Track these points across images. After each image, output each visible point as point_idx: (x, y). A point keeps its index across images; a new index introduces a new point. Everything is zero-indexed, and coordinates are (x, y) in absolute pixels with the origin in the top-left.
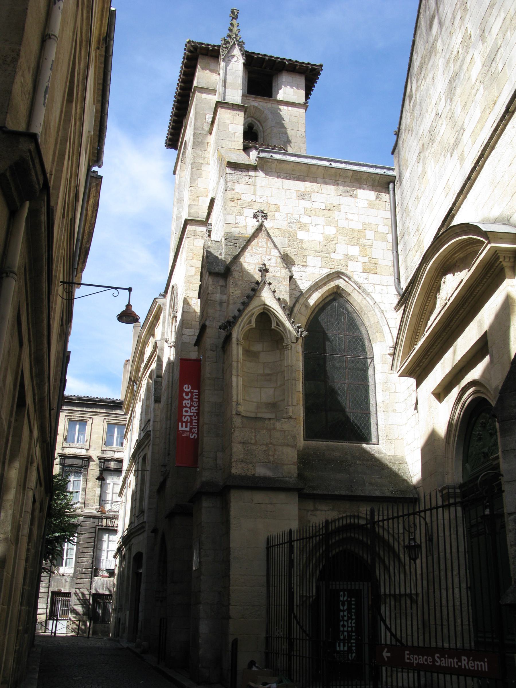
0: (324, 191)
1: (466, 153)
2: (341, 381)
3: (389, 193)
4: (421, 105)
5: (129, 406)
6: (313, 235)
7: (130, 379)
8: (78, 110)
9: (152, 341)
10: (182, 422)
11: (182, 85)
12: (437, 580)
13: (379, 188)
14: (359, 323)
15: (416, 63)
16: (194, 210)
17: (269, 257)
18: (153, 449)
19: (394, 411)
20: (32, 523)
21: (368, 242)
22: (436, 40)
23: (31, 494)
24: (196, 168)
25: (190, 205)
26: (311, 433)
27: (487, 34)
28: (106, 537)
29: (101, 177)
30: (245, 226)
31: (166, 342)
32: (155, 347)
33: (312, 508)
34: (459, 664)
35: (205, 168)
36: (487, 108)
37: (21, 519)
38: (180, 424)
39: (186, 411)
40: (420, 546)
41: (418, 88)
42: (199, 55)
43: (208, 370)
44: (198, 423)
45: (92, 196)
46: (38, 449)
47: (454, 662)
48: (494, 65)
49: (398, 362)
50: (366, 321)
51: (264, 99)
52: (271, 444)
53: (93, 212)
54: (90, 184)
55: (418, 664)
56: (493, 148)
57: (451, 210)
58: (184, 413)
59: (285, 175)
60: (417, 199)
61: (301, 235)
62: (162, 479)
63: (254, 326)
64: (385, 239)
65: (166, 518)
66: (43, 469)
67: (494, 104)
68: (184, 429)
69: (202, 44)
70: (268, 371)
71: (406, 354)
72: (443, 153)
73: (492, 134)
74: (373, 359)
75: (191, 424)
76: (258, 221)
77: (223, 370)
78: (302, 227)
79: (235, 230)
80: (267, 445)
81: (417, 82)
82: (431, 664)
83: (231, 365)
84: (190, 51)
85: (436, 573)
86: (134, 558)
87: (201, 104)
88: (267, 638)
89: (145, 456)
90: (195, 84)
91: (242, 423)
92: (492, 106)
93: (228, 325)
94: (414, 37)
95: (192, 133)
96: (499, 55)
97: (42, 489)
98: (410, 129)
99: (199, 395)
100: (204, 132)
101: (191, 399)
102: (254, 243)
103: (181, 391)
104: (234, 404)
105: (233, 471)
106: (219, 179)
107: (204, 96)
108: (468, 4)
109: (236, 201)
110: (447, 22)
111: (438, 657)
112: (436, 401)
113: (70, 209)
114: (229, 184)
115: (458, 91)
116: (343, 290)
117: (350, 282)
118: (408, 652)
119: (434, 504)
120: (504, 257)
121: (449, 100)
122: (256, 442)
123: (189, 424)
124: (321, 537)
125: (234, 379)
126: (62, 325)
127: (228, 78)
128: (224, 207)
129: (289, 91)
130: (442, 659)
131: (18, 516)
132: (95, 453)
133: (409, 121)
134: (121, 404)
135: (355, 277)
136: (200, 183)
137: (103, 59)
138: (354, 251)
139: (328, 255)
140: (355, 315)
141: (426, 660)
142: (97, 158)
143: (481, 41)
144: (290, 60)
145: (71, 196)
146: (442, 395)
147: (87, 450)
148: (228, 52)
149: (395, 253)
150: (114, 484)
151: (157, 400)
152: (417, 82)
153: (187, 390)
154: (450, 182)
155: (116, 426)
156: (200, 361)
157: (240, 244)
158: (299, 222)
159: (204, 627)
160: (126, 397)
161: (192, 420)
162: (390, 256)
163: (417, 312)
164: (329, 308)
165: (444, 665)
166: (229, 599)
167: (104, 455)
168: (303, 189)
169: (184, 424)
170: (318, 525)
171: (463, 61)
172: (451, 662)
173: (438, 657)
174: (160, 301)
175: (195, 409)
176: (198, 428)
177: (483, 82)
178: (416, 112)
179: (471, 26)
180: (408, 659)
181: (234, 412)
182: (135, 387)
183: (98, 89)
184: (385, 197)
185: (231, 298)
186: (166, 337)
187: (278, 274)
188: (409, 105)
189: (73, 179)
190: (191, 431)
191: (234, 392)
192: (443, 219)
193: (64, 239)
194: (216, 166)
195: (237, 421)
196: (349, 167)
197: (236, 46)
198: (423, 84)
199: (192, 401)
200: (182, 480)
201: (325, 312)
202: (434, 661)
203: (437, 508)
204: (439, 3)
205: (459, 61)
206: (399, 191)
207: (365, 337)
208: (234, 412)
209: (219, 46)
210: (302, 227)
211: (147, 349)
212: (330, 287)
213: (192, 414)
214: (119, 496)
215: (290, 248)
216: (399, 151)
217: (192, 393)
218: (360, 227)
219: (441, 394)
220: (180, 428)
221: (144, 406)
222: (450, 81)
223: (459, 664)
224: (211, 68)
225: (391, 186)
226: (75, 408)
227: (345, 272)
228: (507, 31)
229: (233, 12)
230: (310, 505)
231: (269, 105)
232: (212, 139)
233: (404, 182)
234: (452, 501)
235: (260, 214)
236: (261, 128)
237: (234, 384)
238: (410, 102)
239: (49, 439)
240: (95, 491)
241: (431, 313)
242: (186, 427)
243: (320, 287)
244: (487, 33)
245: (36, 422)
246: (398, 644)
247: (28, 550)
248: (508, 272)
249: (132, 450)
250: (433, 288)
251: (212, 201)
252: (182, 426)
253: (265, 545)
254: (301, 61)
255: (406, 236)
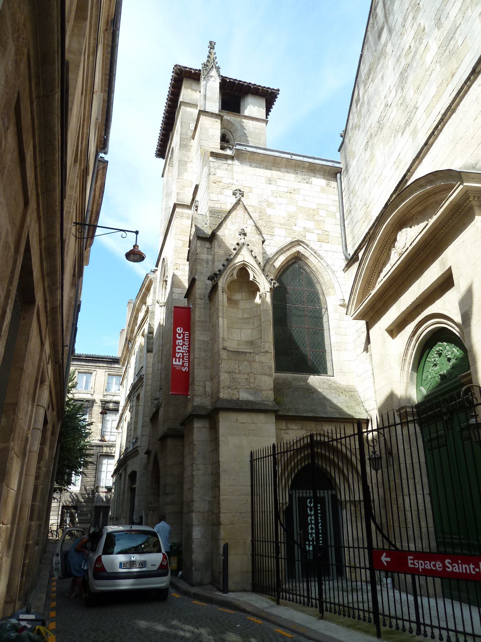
0: (286, 178)
1: (419, 127)
2: (298, 329)
3: (337, 181)
4: (369, 103)
5: (125, 360)
6: (278, 213)
7: (126, 339)
8: (89, 85)
9: (144, 308)
10: (176, 358)
11: (170, 103)
12: (399, 487)
13: (329, 178)
14: (315, 281)
15: (364, 70)
16: (181, 197)
17: (246, 226)
18: (146, 389)
19: (346, 349)
20: (43, 443)
21: (322, 219)
22: (385, 45)
23: (42, 411)
24: (183, 164)
25: (178, 193)
26: (279, 368)
27: (443, 20)
28: (105, 461)
29: (107, 162)
30: (225, 203)
31: (158, 302)
32: (147, 312)
33: (285, 428)
34: (477, 570)
35: (189, 165)
36: (444, 81)
37: (29, 432)
38: (174, 359)
39: (179, 349)
40: (380, 458)
41: (365, 91)
42: (183, 77)
43: (198, 315)
44: (189, 358)
45: (99, 177)
46: (50, 366)
47: (470, 568)
48: (452, 42)
49: (352, 308)
50: (321, 279)
51: (235, 115)
52: (252, 373)
53: (100, 194)
54: (98, 166)
55: (424, 569)
56: (454, 111)
57: (405, 176)
58: (177, 351)
59: (256, 165)
60: (365, 180)
61: (269, 211)
62: (154, 410)
63: (236, 278)
64: (334, 216)
65: (159, 440)
66: (56, 394)
67: (453, 76)
68: (177, 363)
69: (186, 68)
70: (246, 316)
71: (360, 301)
72: (393, 135)
73: (454, 98)
74: (327, 309)
75: (183, 359)
76: (236, 197)
77: (210, 315)
78: (270, 205)
79: (217, 206)
80: (248, 374)
81: (365, 86)
82: (441, 569)
83: (218, 309)
84: (176, 73)
85: (398, 481)
86: (129, 476)
87: (186, 115)
88: (253, 541)
89: (139, 395)
90: (181, 99)
91: (228, 356)
92: (450, 79)
93: (214, 277)
94: (362, 52)
95: (179, 138)
96: (458, 32)
97: (55, 413)
98: (357, 127)
99: (189, 336)
100: (189, 138)
101: (183, 339)
102: (234, 214)
103: (175, 332)
104: (221, 340)
105: (221, 396)
106: (203, 168)
107: (188, 109)
108: (421, 5)
109: (217, 183)
110: (398, 27)
111: (448, 562)
112: (389, 336)
113: (83, 158)
114: (212, 169)
115: (410, 79)
116: (303, 255)
117: (308, 249)
118: (412, 557)
119: (392, 422)
120: (474, 197)
121: (400, 89)
122: (240, 371)
123: (181, 359)
124: (292, 452)
125: (221, 320)
126: (74, 275)
127: (209, 94)
128: (208, 187)
129: (253, 108)
130: (454, 565)
131: (26, 428)
132: (98, 397)
133: (356, 120)
134: (118, 360)
135: (312, 245)
136: (186, 176)
137: (110, 49)
138: (311, 225)
139: (290, 228)
140: (312, 275)
141: (434, 565)
142: (103, 145)
143: (436, 28)
144: (255, 85)
145: (84, 144)
146: (395, 332)
147: (92, 395)
148: (208, 73)
149: (342, 227)
150: (112, 420)
151: (149, 351)
152: (365, 86)
153: (179, 332)
154: (401, 157)
155: (115, 377)
156: (190, 308)
157: (222, 216)
158: (267, 201)
159: (197, 533)
160: (122, 354)
161: (183, 356)
162: (338, 229)
163: (371, 265)
164: (291, 268)
165: (458, 571)
166: (219, 508)
167: (105, 399)
168: (270, 176)
169: (177, 359)
170: (288, 442)
171: (416, 52)
172: (466, 568)
173: (448, 562)
174: (151, 276)
175: (186, 347)
176: (189, 363)
177: (440, 62)
178: (364, 110)
179: (425, 20)
180: (411, 564)
181: (221, 347)
182: (130, 345)
183: (106, 79)
184: (334, 184)
185: (216, 257)
186: (157, 299)
187: (253, 239)
188: (356, 107)
189: (85, 123)
190: (183, 365)
191: (221, 330)
192: (396, 185)
193: (77, 184)
194: (199, 160)
195: (224, 354)
196: (306, 159)
197: (214, 68)
198: (371, 85)
199: (184, 341)
200: (176, 408)
201: (288, 272)
202: (445, 566)
203: (395, 425)
204: (388, 16)
205: (411, 55)
206: (346, 179)
207: (320, 292)
208: (221, 347)
209: (200, 70)
210: (270, 205)
211: (140, 314)
212: (292, 252)
213: (184, 351)
214: (117, 429)
215: (261, 221)
216: (345, 147)
217: (184, 334)
218: (314, 206)
219: (395, 330)
220: (174, 363)
221: (138, 357)
222: (401, 73)
223: (477, 570)
224: (193, 88)
225: (338, 175)
226: (83, 364)
227: (304, 240)
228: (467, 9)
229: (211, 43)
230: (283, 425)
231: (239, 119)
232: (194, 143)
233: (351, 170)
234: (410, 418)
235: (238, 192)
236: (232, 137)
237: (221, 324)
238: (357, 105)
239: (61, 361)
240: (98, 426)
241: (384, 265)
242: (179, 361)
243: (284, 252)
244: (444, 19)
245: (48, 338)
246: (393, 548)
247: (38, 468)
248: (476, 210)
249: (128, 392)
250: (390, 241)
251: (197, 187)
252: (176, 361)
253: (249, 459)
254: (263, 86)
255: (353, 212)
